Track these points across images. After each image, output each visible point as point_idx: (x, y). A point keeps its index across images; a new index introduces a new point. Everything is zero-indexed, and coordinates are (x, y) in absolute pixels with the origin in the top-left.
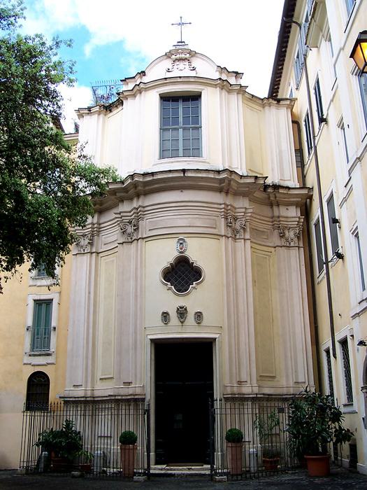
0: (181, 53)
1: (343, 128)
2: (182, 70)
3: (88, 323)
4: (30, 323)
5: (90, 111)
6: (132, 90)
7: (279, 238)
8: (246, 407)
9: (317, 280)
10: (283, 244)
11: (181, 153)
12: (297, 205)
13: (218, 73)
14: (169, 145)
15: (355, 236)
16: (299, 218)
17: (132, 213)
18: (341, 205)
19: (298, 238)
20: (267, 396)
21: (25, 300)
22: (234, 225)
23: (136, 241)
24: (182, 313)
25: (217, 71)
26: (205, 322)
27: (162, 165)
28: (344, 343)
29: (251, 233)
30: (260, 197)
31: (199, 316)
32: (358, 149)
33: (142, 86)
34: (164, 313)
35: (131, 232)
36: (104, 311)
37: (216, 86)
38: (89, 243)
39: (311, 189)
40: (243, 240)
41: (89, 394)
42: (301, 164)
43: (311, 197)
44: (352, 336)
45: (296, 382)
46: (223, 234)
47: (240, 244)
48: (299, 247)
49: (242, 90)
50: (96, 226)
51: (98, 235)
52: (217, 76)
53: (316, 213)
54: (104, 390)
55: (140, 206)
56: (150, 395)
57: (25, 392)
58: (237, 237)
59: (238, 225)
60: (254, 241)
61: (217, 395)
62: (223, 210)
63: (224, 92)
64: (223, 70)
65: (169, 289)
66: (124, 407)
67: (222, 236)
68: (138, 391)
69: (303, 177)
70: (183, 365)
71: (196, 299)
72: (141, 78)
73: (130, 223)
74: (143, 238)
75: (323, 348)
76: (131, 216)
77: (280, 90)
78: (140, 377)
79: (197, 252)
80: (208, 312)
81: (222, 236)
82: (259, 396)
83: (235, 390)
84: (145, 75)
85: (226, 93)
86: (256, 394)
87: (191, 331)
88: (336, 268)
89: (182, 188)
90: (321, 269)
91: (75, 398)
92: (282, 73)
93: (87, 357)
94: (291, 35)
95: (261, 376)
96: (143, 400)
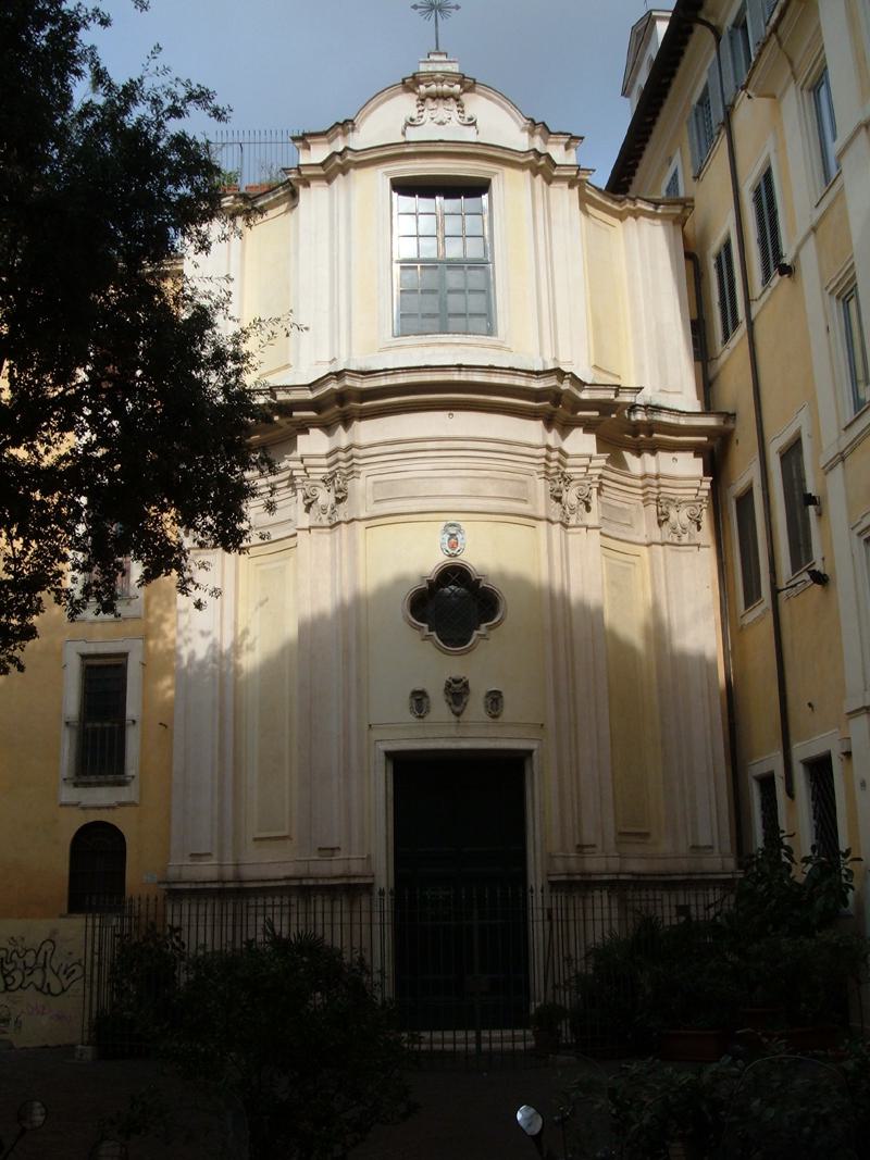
6: (322, 165)
12: (697, 450)
13: (527, 134)
24: (457, 692)
26: (508, 713)
31: (495, 700)
41: (229, 873)
44: (848, 754)
45: (693, 847)
46: (541, 513)
47: (577, 538)
56: (383, 877)
58: (572, 522)
61: (536, 878)
65: (426, 638)
67: (540, 520)
68: (356, 867)
71: (488, 660)
75: (758, 768)
78: (363, 835)
82: (622, 877)
83: (573, 864)
87: (477, 735)
91: (196, 882)
94: (689, 51)
96: (369, 888)
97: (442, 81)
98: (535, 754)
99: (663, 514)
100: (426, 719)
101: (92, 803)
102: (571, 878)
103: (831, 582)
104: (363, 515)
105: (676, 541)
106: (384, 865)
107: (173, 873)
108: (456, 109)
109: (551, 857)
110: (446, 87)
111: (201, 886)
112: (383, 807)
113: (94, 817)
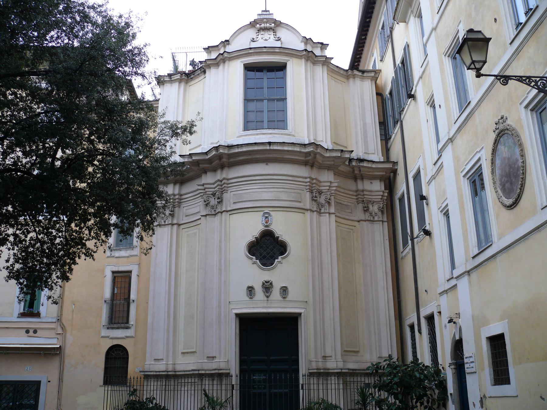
0: (266, 24)
1: (433, 106)
2: (267, 40)
3: (169, 296)
4: (107, 294)
5: (171, 78)
6: (216, 59)
7: (363, 212)
8: (329, 382)
9: (400, 256)
10: (367, 218)
11: (266, 124)
12: (381, 178)
13: (303, 43)
14: (252, 116)
15: (444, 214)
16: (383, 192)
17: (216, 185)
18: (429, 183)
19: (382, 212)
20: (352, 371)
21: (103, 271)
22: (318, 199)
23: (220, 214)
24: (267, 287)
25: (302, 42)
26: (290, 297)
27: (247, 137)
28: (430, 319)
29: (335, 206)
30: (344, 170)
31: (284, 290)
32: (449, 130)
33: (226, 55)
34: (249, 287)
35: (215, 203)
36: (187, 284)
37: (300, 57)
38: (170, 214)
39: (395, 163)
40: (328, 214)
41: (170, 368)
42: (386, 137)
43: (395, 172)
44: (440, 312)
45: (379, 357)
46: (308, 207)
47: (325, 218)
48: (383, 222)
49: (327, 61)
50: (177, 197)
51: (179, 207)
52: (301, 46)
53: (401, 188)
54: (186, 364)
55: (224, 179)
56: (234, 369)
57: (103, 366)
58: (322, 211)
59: (322, 200)
60: (338, 214)
61: (303, 370)
62: (308, 184)
63: (309, 63)
64: (307, 41)
65: (254, 263)
66: (207, 383)
67: (307, 210)
68: (223, 365)
69: (387, 150)
70: (268, 339)
71: (282, 272)
72: (225, 46)
73: (214, 195)
74: (227, 211)
76: (214, 188)
77: (362, 60)
78: (224, 352)
79: (283, 227)
80: (292, 286)
81: (307, 210)
82: (344, 371)
83: (321, 365)
84: (228, 44)
85: (311, 64)
86: (341, 369)
87: (276, 306)
88: (422, 245)
89: (267, 161)
90: (405, 244)
91: (156, 372)
92: (364, 43)
93: (168, 331)
95: (345, 351)
97: (267, 23)
98: (302, 314)
99: (365, 207)
100: (254, 299)
101: (115, 336)
102: (319, 371)
103: (432, 235)
104: (229, 209)
105: (372, 219)
106: (234, 364)
107: (147, 368)
108: (272, 34)
109: (311, 361)
110: (268, 25)
111: (158, 373)
112: (234, 338)
113: (116, 342)
